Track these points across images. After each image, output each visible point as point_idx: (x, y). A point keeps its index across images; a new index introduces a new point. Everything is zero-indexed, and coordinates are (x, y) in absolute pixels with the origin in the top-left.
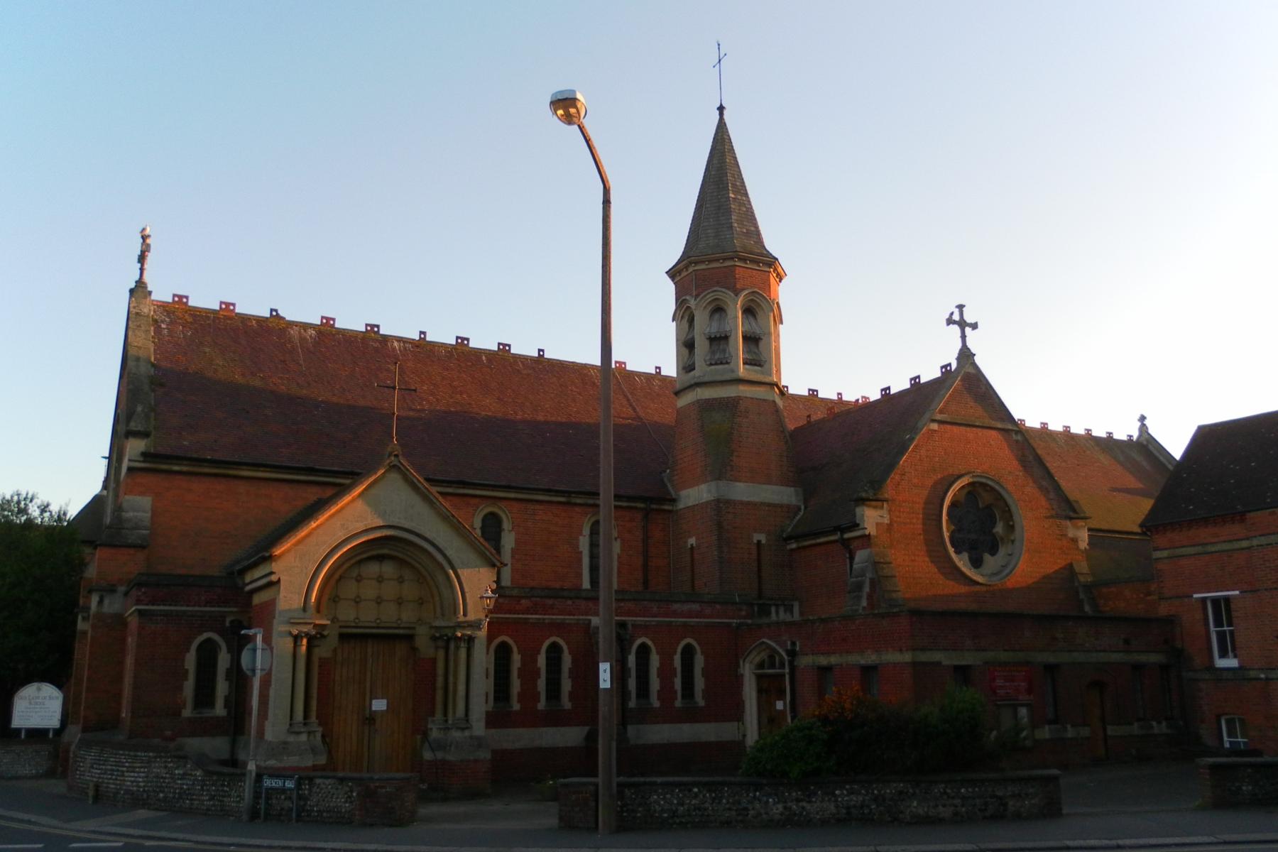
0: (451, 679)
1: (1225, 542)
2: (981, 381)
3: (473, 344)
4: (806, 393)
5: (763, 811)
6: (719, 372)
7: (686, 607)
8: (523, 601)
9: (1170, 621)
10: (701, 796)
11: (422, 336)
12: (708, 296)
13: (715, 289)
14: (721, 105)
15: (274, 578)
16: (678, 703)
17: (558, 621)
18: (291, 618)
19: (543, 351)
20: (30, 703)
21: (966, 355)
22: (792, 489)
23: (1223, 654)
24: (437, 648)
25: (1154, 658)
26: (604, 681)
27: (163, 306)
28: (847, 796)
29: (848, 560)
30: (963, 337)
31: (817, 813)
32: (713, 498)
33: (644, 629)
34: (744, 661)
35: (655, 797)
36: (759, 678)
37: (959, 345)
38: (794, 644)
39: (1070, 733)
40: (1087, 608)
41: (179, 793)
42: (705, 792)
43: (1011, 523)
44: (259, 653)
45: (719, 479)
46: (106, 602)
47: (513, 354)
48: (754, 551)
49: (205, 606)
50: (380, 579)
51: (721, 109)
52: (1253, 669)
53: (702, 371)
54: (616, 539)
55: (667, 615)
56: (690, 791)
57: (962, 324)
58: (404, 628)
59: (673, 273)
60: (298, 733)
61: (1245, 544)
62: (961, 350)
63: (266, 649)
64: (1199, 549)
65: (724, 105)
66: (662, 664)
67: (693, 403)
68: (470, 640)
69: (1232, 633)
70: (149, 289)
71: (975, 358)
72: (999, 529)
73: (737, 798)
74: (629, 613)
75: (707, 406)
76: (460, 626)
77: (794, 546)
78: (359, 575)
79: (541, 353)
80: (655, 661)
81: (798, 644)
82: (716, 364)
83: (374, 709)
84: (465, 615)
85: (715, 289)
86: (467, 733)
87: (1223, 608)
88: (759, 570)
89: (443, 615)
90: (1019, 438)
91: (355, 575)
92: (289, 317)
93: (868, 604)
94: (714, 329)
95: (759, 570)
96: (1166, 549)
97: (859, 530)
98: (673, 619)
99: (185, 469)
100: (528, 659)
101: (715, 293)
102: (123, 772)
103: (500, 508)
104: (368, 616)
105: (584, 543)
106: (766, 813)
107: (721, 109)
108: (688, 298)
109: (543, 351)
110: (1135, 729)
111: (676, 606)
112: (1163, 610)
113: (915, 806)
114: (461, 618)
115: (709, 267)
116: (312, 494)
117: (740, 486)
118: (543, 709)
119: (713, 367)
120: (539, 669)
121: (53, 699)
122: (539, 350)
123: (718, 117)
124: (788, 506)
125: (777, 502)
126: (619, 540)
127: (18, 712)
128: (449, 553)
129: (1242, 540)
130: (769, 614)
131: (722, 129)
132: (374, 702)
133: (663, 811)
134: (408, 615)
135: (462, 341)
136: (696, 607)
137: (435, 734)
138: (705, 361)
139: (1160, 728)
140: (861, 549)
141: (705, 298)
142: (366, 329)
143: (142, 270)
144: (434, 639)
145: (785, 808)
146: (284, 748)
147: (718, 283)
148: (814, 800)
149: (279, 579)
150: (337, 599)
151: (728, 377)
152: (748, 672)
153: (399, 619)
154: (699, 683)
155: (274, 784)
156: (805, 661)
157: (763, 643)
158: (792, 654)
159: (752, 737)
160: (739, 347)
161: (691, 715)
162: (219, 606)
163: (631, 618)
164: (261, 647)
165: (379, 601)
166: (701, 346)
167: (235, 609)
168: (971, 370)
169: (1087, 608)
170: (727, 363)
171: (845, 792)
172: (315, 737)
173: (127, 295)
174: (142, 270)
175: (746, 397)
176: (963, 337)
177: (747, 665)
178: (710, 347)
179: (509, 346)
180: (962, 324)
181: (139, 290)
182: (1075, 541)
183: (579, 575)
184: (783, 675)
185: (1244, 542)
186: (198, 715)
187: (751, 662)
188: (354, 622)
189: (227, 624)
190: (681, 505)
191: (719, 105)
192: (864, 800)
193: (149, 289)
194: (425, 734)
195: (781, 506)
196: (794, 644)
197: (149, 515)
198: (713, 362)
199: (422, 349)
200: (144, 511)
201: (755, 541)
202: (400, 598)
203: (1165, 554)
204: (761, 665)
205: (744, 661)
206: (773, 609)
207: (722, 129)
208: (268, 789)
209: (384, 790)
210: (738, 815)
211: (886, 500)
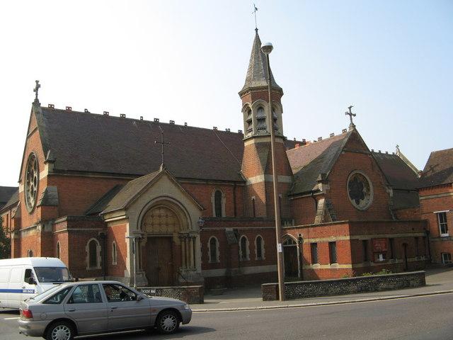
0: (187, 253)
4: (153, 120)
9: (426, 222)
23: (443, 232)
24: (181, 241)
25: (421, 234)
30: (351, 119)
33: (243, 232)
38: (300, 235)
39: (397, 261)
51: (257, 30)
55: (251, 226)
57: (351, 114)
64: (440, 196)
66: (250, 244)
69: (446, 225)
72: (365, 190)
76: (191, 232)
80: (99, 248)
94: (259, 116)
104: (157, 230)
105: (213, 199)
107: (257, 30)
110: (416, 259)
112: (423, 218)
116: (114, 183)
128: (186, 206)
134: (170, 229)
135: (69, 108)
137: (183, 273)
139: (423, 259)
143: (37, 94)
144: (180, 237)
154: (218, 254)
156: (305, 241)
161: (261, 263)
165: (160, 224)
174: (37, 94)
176: (351, 119)
180: (351, 114)
182: (389, 194)
195: (287, 183)
196: (300, 235)
199: (142, 123)
203: (424, 198)
204: (286, 243)
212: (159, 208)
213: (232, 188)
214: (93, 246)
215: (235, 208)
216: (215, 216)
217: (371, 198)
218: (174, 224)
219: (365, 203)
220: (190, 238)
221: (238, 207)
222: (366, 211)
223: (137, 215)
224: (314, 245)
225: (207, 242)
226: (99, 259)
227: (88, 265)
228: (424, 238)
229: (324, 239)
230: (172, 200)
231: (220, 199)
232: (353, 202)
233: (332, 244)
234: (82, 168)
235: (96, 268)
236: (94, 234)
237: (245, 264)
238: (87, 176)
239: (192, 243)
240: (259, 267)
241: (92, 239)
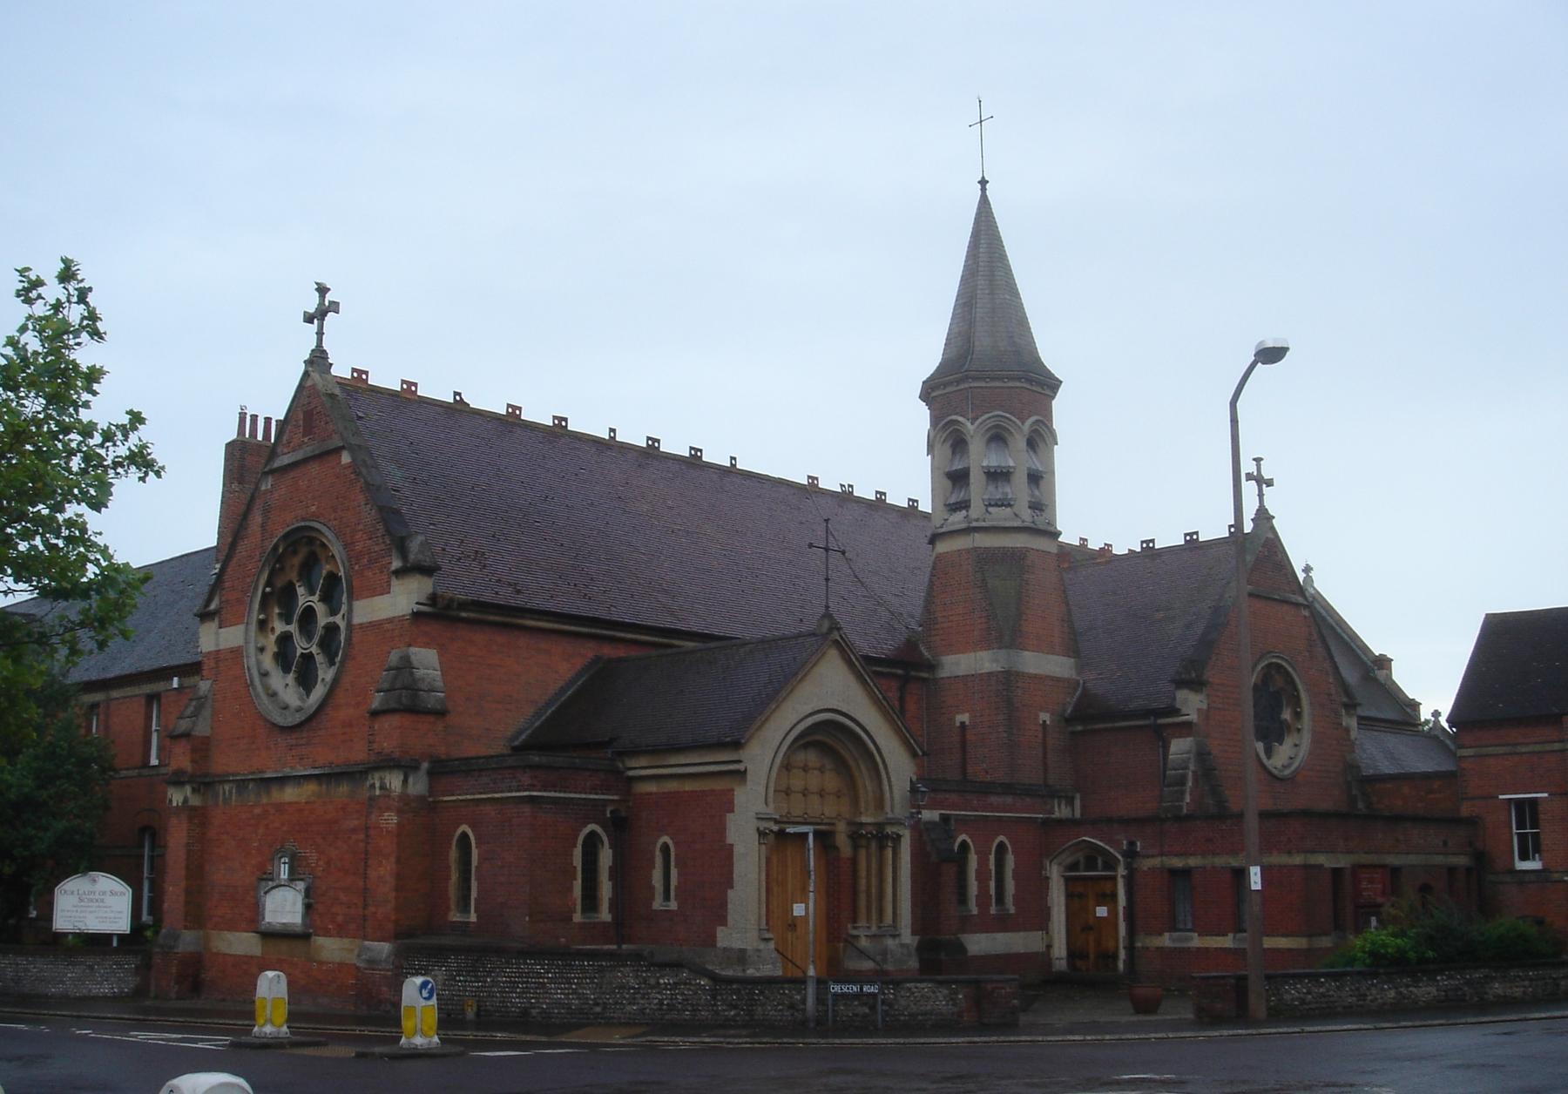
1: (1536, 743)
3: (373, 381)
5: (1378, 996)
6: (1000, 516)
9: (1472, 822)
10: (1327, 985)
14: (983, 177)
15: (741, 767)
16: (993, 910)
18: (757, 814)
19: (735, 459)
20: (81, 900)
22: (1073, 660)
25: (1462, 861)
26: (1255, 882)
27: (341, 382)
28: (1446, 980)
29: (1161, 750)
30: (1261, 495)
32: (1000, 669)
33: (963, 821)
34: (1051, 862)
36: (1068, 881)
38: (1132, 844)
40: (1361, 805)
41: (668, 1004)
43: (1299, 710)
46: (411, 780)
47: (419, 396)
48: (1040, 729)
49: (590, 793)
51: (983, 182)
52: (1557, 872)
56: (1317, 981)
60: (767, 940)
61: (1557, 746)
62: (1258, 510)
65: (987, 179)
67: (968, 551)
68: (897, 838)
69: (1536, 836)
70: (330, 361)
71: (1274, 521)
72: (1286, 715)
73: (1357, 985)
74: (954, 807)
75: (986, 559)
77: (1079, 728)
79: (733, 462)
80: (606, 857)
81: (1138, 844)
83: (795, 914)
84: (892, 811)
86: (897, 941)
87: (1528, 812)
88: (1045, 754)
93: (1191, 800)
95: (1045, 754)
96: (1470, 747)
99: (472, 615)
100: (983, 862)
101: (1000, 419)
102: (544, 983)
106: (1382, 998)
107: (983, 182)
108: (960, 419)
109: (735, 459)
111: (993, 799)
112: (1466, 810)
113: (1497, 988)
114: (890, 815)
117: (1027, 655)
120: (675, 867)
121: (116, 894)
123: (980, 192)
124: (1068, 681)
125: (1059, 676)
127: (63, 911)
129: (1555, 742)
131: (984, 202)
132: (795, 906)
135: (410, 386)
136: (1009, 800)
138: (983, 500)
140: (1177, 737)
141: (985, 424)
143: (320, 334)
146: (758, 956)
149: (746, 769)
150: (806, 792)
152: (1055, 874)
153: (823, 814)
154: (1010, 886)
155: (846, 990)
157: (1084, 841)
158: (1131, 854)
159: (1060, 950)
161: (1003, 923)
162: (603, 794)
165: (805, 793)
167: (616, 797)
168: (1271, 535)
169: (1361, 805)
174: (320, 334)
175: (1033, 549)
176: (1261, 495)
181: (318, 359)
184: (1114, 879)
185: (1556, 744)
186: (587, 921)
187: (1060, 864)
189: (608, 815)
191: (980, 179)
193: (330, 361)
194: (851, 941)
196: (1132, 844)
197: (439, 673)
198: (993, 503)
199: (609, 447)
204: (1073, 867)
205: (1051, 862)
207: (984, 202)
208: (835, 994)
209: (1003, 991)
210: (1358, 1001)
214: (592, 844)
217: (1306, 740)
219: (1287, 755)
220: (887, 837)
222: (1291, 779)
223: (768, 761)
226: (606, 889)
227: (579, 907)
228: (1468, 870)
229: (1220, 861)
232: (1260, 746)
234: (505, 596)
235: (452, 913)
236: (592, 811)
237: (968, 924)
238: (520, 621)
239: (889, 853)
240: (1000, 936)
241: (599, 829)
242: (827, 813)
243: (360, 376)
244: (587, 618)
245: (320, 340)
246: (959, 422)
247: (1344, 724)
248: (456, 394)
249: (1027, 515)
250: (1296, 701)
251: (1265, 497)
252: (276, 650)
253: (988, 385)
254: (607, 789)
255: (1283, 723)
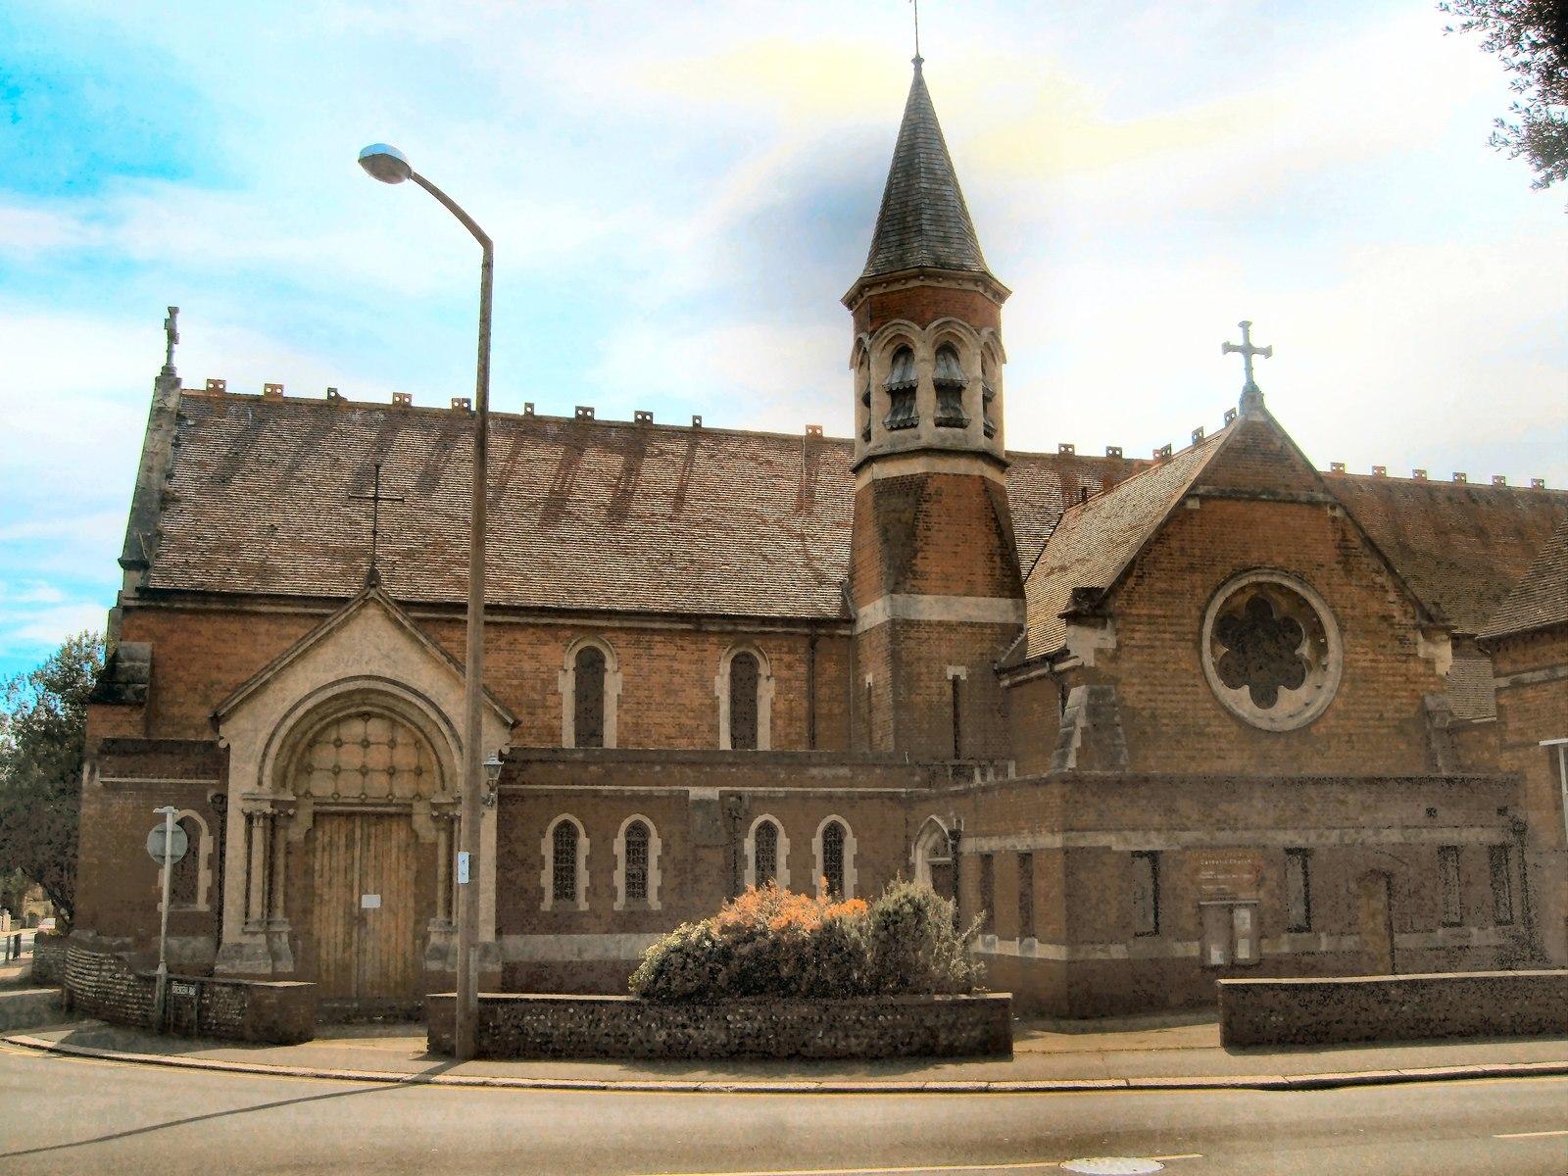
2: (1275, 434)
4: (572, 415)
6: (906, 439)
7: (828, 772)
8: (592, 768)
11: (529, 409)
12: (886, 334)
13: (894, 321)
14: (918, 55)
17: (642, 794)
18: (243, 794)
19: (700, 418)
21: (1252, 396)
22: (1010, 601)
28: (739, 1022)
30: (1249, 369)
31: (705, 1043)
33: (769, 801)
35: (529, 1018)
37: (1243, 382)
42: (582, 1013)
43: (1322, 641)
44: (169, 835)
45: (893, 591)
50: (365, 744)
51: (918, 61)
53: (928, 432)
54: (768, 678)
56: (566, 1010)
57: (1248, 350)
58: (397, 805)
59: (850, 302)
60: (254, 934)
63: (179, 832)
72: (1305, 650)
78: (338, 739)
82: (899, 428)
83: (364, 906)
85: (894, 321)
89: (444, 788)
90: (1338, 513)
91: (334, 736)
92: (351, 398)
97: (1070, 659)
98: (809, 789)
101: (895, 328)
103: (602, 642)
107: (918, 61)
109: (700, 418)
115: (888, 290)
118: (621, 909)
119: (896, 433)
122: (695, 418)
123: (913, 73)
124: (1003, 626)
126: (772, 681)
130: (970, 778)
131: (919, 85)
133: (537, 1034)
134: (403, 788)
136: (844, 771)
142: (453, 405)
143: (170, 352)
144: (435, 819)
145: (669, 1035)
146: (236, 952)
147: (899, 314)
148: (701, 1026)
149: (229, 745)
151: (912, 445)
153: (391, 794)
154: (654, 878)
156: (969, 846)
160: (926, 403)
163: (747, 789)
164: (171, 829)
165: (364, 771)
166: (881, 402)
167: (214, 782)
170: (914, 426)
171: (738, 1017)
172: (280, 937)
173: (154, 382)
176: (1249, 369)
177: (919, 852)
178: (893, 404)
179: (651, 414)
180: (1248, 350)
181: (167, 378)
183: (715, 729)
188: (332, 797)
190: (859, 630)
192: (760, 1030)
195: (992, 625)
200: (143, 661)
201: (950, 677)
202: (393, 767)
204: (935, 852)
206: (977, 772)
207: (919, 85)
211: (1111, 616)
212: (366, 716)
213: (806, 642)
215: (812, 717)
216: (725, 744)
218: (419, 772)
221: (823, 709)
224: (987, 859)
225: (543, 833)
230: (390, 688)
231: (755, 686)
233: (1025, 858)
235: (191, 908)
241: (834, 817)
242: (398, 793)
243: (1114, 452)
244: (555, 610)
245: (169, 358)
246: (954, 322)
247: (1421, 654)
248: (330, 390)
249: (981, 443)
250: (1318, 631)
251: (1244, 367)
252: (1283, 691)
253: (904, 287)
254: (204, 773)
255: (1298, 661)
